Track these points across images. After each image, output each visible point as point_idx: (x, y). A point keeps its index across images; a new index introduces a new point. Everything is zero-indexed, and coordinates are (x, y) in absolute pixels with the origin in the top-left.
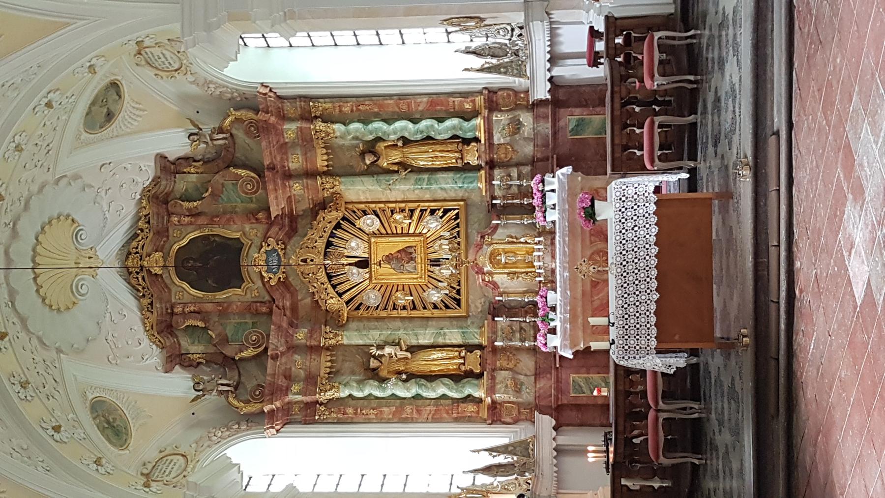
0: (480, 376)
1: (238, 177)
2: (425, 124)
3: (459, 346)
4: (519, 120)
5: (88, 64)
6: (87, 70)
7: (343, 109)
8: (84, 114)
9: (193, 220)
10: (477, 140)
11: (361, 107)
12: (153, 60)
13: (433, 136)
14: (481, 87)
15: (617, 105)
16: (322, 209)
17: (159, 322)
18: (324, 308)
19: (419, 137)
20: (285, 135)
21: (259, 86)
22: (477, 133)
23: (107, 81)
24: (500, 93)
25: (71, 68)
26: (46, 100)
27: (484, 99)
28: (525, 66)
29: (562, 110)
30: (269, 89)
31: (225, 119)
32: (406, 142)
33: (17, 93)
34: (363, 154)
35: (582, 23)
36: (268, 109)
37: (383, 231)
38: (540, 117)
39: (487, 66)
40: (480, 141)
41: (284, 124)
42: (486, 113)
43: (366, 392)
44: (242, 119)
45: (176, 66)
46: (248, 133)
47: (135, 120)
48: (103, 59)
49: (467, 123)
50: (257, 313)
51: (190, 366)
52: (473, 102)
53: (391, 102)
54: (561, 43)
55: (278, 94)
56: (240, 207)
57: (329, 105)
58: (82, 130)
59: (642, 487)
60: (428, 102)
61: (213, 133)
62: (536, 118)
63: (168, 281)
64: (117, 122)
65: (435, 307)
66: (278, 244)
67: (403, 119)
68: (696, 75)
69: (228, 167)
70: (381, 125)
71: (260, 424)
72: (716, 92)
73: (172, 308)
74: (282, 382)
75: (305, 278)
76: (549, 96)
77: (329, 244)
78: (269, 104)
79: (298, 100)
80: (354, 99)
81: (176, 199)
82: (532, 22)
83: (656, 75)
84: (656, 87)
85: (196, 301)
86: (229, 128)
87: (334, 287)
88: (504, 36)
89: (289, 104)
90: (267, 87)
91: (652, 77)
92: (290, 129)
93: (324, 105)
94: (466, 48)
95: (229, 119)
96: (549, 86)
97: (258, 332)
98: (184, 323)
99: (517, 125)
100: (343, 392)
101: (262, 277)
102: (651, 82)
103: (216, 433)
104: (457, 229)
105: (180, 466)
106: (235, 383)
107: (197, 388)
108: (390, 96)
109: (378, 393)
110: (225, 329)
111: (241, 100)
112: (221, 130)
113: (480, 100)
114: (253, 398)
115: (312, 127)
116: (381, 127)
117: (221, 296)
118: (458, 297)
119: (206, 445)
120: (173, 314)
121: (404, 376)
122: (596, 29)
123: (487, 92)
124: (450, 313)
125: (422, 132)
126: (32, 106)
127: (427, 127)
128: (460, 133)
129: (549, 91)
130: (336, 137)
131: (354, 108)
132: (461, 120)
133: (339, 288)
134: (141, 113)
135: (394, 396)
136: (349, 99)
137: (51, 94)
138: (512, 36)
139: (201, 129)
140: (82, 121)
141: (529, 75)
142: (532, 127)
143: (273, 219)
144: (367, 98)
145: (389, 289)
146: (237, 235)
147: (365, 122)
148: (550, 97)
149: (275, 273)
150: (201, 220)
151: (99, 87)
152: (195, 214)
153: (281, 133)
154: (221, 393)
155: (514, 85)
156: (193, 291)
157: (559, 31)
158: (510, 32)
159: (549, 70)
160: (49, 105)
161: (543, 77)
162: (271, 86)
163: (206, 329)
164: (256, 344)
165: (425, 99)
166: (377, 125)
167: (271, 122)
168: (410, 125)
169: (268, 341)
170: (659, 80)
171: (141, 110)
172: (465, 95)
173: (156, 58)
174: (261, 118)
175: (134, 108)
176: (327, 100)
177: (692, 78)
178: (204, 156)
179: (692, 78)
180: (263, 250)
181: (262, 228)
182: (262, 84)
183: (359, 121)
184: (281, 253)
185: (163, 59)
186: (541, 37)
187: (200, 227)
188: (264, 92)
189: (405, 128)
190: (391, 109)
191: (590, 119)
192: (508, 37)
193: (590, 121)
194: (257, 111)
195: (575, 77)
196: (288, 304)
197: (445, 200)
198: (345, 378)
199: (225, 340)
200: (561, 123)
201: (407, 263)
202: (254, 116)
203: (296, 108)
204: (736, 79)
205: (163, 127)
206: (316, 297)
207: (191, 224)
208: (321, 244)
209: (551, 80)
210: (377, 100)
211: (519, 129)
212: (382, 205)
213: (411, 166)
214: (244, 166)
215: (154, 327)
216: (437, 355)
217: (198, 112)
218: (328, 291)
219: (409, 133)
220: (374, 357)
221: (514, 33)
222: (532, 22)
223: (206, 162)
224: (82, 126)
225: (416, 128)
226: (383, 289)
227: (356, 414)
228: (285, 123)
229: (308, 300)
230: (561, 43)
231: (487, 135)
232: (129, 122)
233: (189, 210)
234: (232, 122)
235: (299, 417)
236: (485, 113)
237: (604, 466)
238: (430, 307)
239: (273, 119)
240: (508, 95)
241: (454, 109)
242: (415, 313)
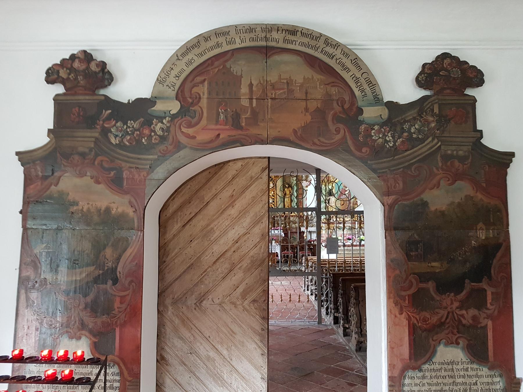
32: (291, 196)
166: (295, 188)
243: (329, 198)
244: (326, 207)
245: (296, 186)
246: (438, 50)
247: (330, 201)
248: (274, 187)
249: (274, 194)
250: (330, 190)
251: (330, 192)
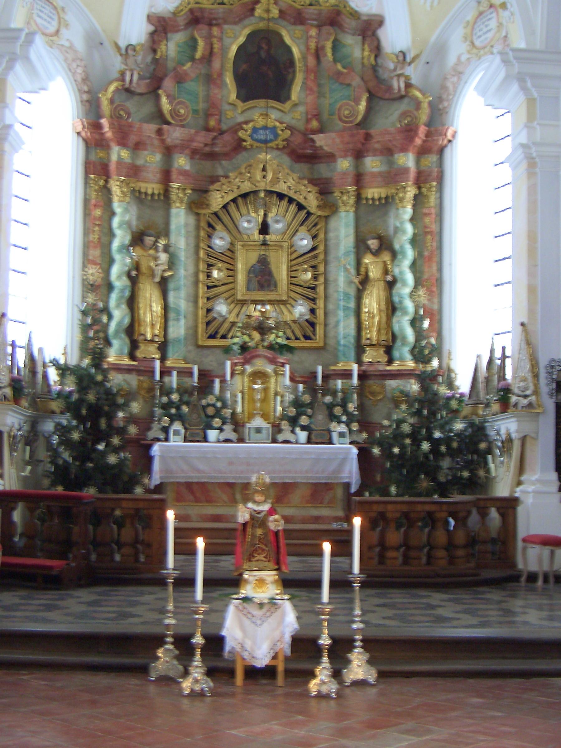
0: (132, 357)
1: (357, 101)
3: (165, 335)
9: (313, 51)
10: (390, 361)
12: (484, 20)
16: (320, 190)
17: (202, 10)
18: (212, 187)
19: (396, 299)
31: (420, 91)
32: (391, 285)
34: (380, 238)
37: (294, 256)
40: (388, 365)
43: (118, 232)
45: (477, 43)
50: (208, 115)
51: (154, 42)
56: (326, 102)
59: (81, 489)
63: (247, 22)
65: (209, 311)
66: (283, 141)
69: (369, 92)
71: (87, 113)
72: (440, 606)
73: (217, 25)
74: (133, 139)
75: (246, 168)
77: (281, 196)
81: (336, 35)
85: (224, 50)
87: (234, 200)
97: (187, 116)
98: (201, 37)
100: (119, 206)
101: (246, 123)
103: (79, 68)
104: (293, 338)
105: (47, 28)
106: (133, 89)
107: (130, 47)
108: (440, 269)
109: (116, 244)
110: (192, 81)
112: (408, 86)
114: (116, 108)
117: (229, 79)
118: (219, 336)
119: (68, 56)
120: (210, 25)
121: (134, 273)
124: (201, 328)
128: (398, 343)
132: (412, 345)
133: (232, 205)
135: (111, 261)
139: (410, 64)
143: (312, 136)
145: (230, 261)
146: (294, 96)
147: (414, 242)
149: (251, 136)
150: (311, 61)
152: (318, 54)
153: (404, 150)
154: (123, 74)
156: (234, 49)
163: (192, 59)
164: (174, 113)
165: (436, 307)
166: (410, 254)
169: (177, 126)
173: (486, 23)
178: (381, 67)
180: (278, 124)
181: (300, 125)
182: (455, 132)
184: (272, 144)
185: (485, 30)
187: (304, 58)
189: (405, 284)
190: (426, 270)
196: (217, 149)
197: (326, 325)
198: (134, 210)
199: (180, 80)
201: (258, 281)
206: (223, 180)
207: (308, 49)
208: (282, 188)
212: (322, 257)
213: (364, 289)
214: (369, 109)
215: (197, 6)
216: (157, 308)
218: (230, 193)
220: (156, 241)
222: (517, 421)
223: (375, 68)
226: (229, 254)
227: (95, 219)
229: (220, 172)
231: (396, 373)
233: (323, 48)
235: (93, 157)
238: (209, 305)
239: (418, 141)
242: (202, 289)
246: (228, 258)
248: (314, 249)
249: (315, 278)
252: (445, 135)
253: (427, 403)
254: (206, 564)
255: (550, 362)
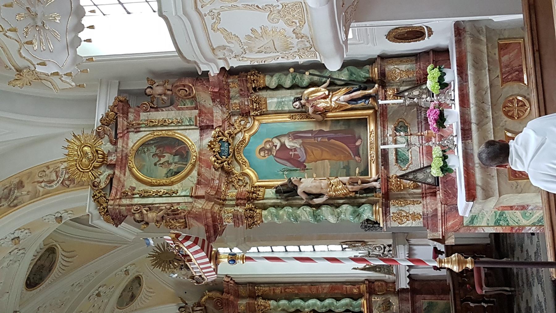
2: (328, 301)
4: (389, 301)
5: (125, 269)
6: (124, 273)
7: (276, 291)
8: (118, 297)
11: (286, 290)
13: (333, 310)
14: (364, 279)
15: (458, 303)
20: (239, 308)
21: (224, 276)
22: (362, 309)
23: (134, 276)
24: (376, 283)
25: (114, 273)
26: (97, 292)
27: (366, 287)
28: (392, 268)
29: (418, 296)
30: (230, 278)
31: (202, 297)
33: (81, 288)
35: (429, 245)
36: (229, 291)
38: (403, 300)
39: (368, 266)
41: (238, 301)
42: (368, 296)
44: (212, 297)
46: (216, 306)
47: (148, 299)
48: (134, 266)
49: (355, 301)
52: (359, 288)
53: (306, 287)
54: (415, 254)
55: (236, 281)
57: (267, 289)
58: (116, 307)
60: (329, 288)
61: (194, 306)
62: (401, 300)
64: (136, 301)
67: (313, 298)
68: (510, 287)
70: (299, 302)
76: (408, 287)
78: (230, 288)
79: (248, 285)
80: (282, 285)
82: (398, 245)
83: (484, 286)
84: (484, 293)
86: (204, 303)
88: (379, 251)
89: (242, 287)
90: (229, 277)
91: (481, 287)
92: (242, 304)
93: (264, 288)
94: (355, 256)
95: (205, 298)
96: (408, 280)
99: (389, 304)
102: (480, 290)
108: (306, 283)
111: (213, 285)
112: (199, 305)
113: (363, 287)
115: (256, 303)
116: (300, 304)
122: (439, 249)
123: (367, 282)
125: (326, 307)
126: (88, 296)
127: (329, 304)
129: (408, 284)
130: (271, 309)
131: (283, 291)
132: (351, 300)
134: (152, 295)
136: (279, 285)
137: (101, 288)
138: (384, 251)
139: (186, 304)
140: (116, 302)
141: (395, 273)
142: (398, 306)
144: (291, 284)
147: (290, 299)
148: (409, 287)
151: (129, 280)
153: (235, 307)
155: (385, 278)
157: (415, 252)
158: (383, 249)
159: (408, 271)
160: (98, 295)
161: (404, 275)
162: (231, 277)
165: (328, 286)
166: (297, 302)
167: (230, 299)
168: (318, 302)
170: (486, 289)
171: (151, 292)
172: (354, 283)
174: (224, 297)
175: (148, 291)
176: (266, 285)
177: (508, 289)
179: (508, 289)
182: (226, 276)
183: (285, 299)
186: (403, 252)
188: (227, 281)
189: (314, 305)
190: (306, 292)
191: (437, 303)
192: (382, 251)
193: (437, 304)
194: (222, 292)
195: (424, 275)
200: (417, 305)
202: (220, 296)
203: (247, 290)
204: (542, 299)
205: (164, 303)
209: (409, 277)
210: (297, 286)
211: (389, 307)
217: (186, 293)
219: (318, 308)
221: (386, 250)
222: (398, 245)
224: (116, 305)
225: (322, 304)
228: (239, 300)
230: (415, 254)
231: (368, 310)
232: (144, 301)
234: (206, 299)
236: (367, 296)
237: (356, 267)
240: (382, 284)
241: (347, 292)
243: (304, 196)
244: (331, 205)
245: (294, 299)
247: (315, 191)
250: (277, 192)
251: (285, 192)
252: (228, 282)
253: (221, 149)
254: (505, 235)
255: (362, 228)
